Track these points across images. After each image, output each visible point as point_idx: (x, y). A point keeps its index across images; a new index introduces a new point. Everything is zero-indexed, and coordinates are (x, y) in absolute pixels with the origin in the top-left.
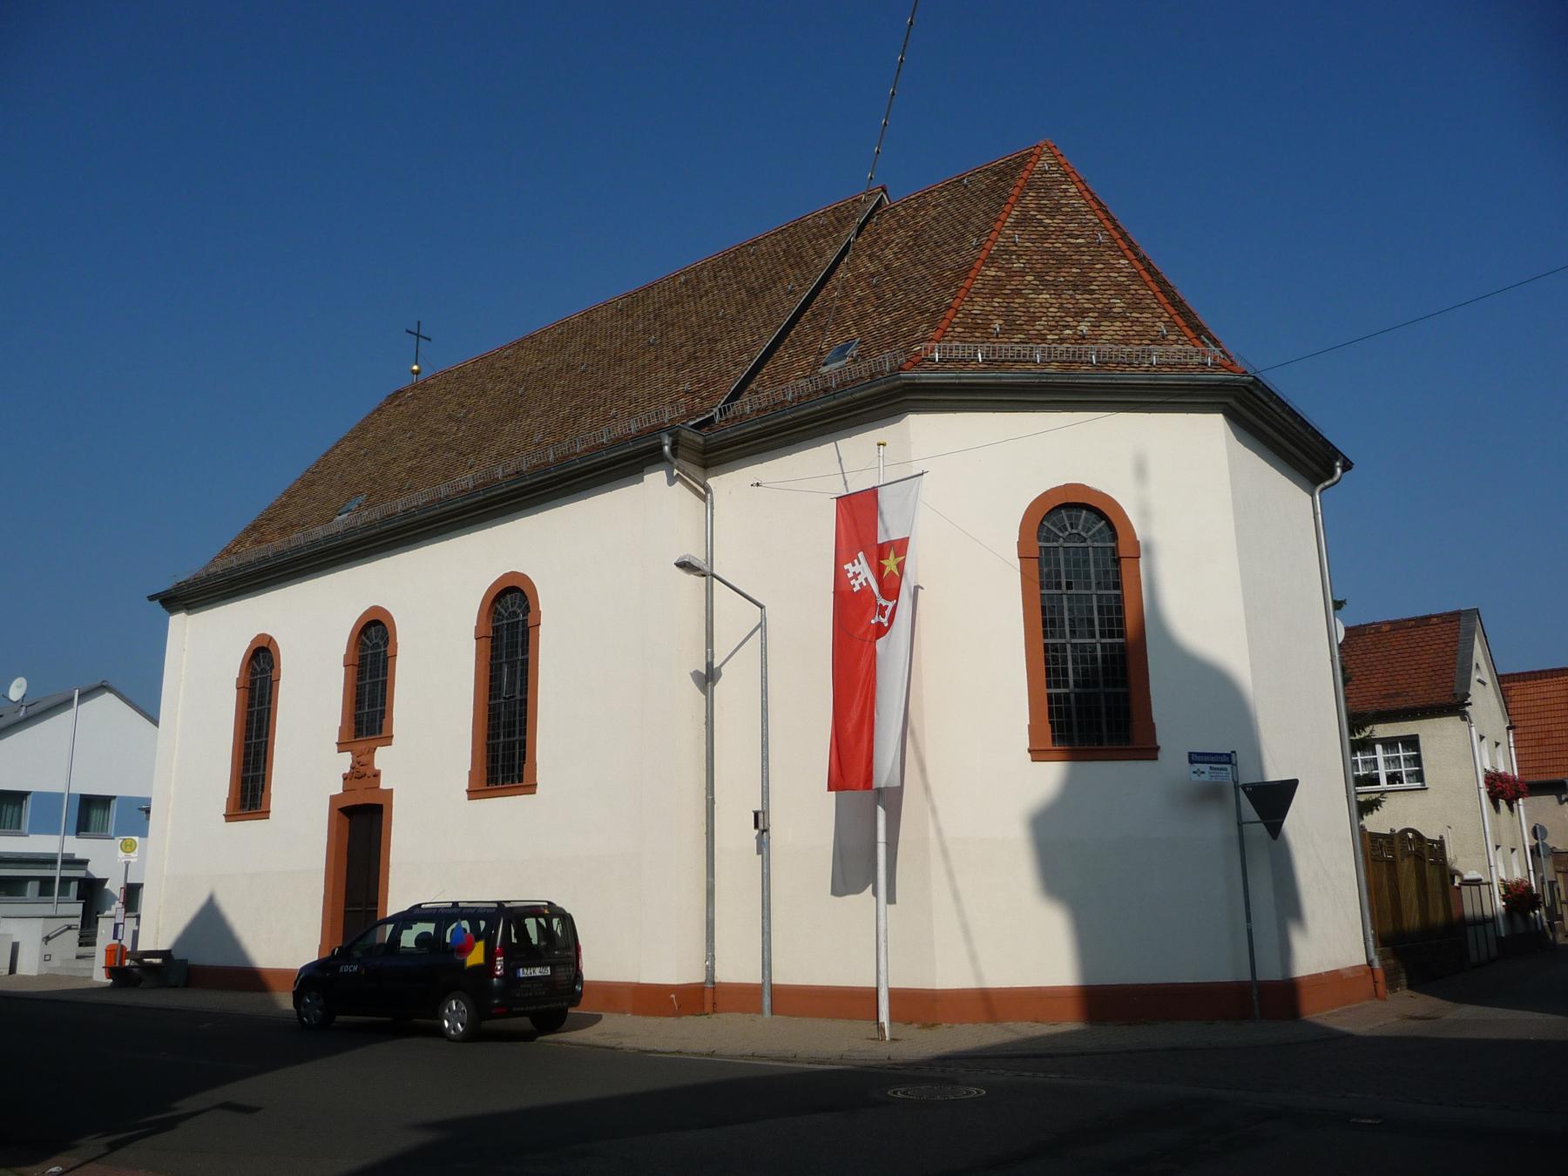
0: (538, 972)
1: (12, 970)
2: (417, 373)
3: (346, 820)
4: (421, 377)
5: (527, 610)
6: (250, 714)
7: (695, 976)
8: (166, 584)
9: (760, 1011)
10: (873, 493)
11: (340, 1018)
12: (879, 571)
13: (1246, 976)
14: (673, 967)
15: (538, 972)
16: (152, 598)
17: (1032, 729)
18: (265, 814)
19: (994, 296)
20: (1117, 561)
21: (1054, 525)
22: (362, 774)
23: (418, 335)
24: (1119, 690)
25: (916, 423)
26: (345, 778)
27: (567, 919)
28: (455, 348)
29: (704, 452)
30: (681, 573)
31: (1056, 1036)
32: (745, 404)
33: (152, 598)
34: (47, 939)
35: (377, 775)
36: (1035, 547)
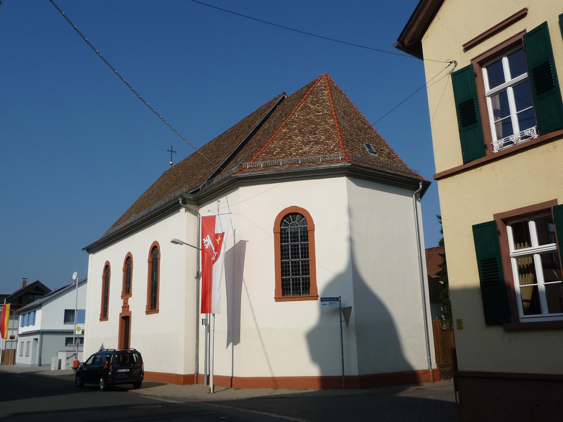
0: (124, 370)
1: (60, 368)
2: (172, 164)
3: (124, 321)
4: (173, 166)
5: (305, 222)
6: (129, 284)
7: (192, 372)
8: (87, 244)
9: (204, 383)
10: (214, 217)
11: (86, 384)
12: (215, 243)
13: (339, 373)
14: (181, 368)
15: (124, 370)
16: (83, 249)
17: (276, 291)
18: (157, 311)
19: (281, 140)
20: (307, 232)
21: (287, 221)
22: (126, 307)
23: (172, 151)
24: (298, 277)
25: (241, 189)
26: (122, 307)
27: (139, 354)
28: (184, 153)
29: (197, 201)
30: (174, 245)
31: (307, 393)
32: (215, 180)
33: (83, 249)
34: (68, 358)
35: (128, 307)
36: (158, 256)
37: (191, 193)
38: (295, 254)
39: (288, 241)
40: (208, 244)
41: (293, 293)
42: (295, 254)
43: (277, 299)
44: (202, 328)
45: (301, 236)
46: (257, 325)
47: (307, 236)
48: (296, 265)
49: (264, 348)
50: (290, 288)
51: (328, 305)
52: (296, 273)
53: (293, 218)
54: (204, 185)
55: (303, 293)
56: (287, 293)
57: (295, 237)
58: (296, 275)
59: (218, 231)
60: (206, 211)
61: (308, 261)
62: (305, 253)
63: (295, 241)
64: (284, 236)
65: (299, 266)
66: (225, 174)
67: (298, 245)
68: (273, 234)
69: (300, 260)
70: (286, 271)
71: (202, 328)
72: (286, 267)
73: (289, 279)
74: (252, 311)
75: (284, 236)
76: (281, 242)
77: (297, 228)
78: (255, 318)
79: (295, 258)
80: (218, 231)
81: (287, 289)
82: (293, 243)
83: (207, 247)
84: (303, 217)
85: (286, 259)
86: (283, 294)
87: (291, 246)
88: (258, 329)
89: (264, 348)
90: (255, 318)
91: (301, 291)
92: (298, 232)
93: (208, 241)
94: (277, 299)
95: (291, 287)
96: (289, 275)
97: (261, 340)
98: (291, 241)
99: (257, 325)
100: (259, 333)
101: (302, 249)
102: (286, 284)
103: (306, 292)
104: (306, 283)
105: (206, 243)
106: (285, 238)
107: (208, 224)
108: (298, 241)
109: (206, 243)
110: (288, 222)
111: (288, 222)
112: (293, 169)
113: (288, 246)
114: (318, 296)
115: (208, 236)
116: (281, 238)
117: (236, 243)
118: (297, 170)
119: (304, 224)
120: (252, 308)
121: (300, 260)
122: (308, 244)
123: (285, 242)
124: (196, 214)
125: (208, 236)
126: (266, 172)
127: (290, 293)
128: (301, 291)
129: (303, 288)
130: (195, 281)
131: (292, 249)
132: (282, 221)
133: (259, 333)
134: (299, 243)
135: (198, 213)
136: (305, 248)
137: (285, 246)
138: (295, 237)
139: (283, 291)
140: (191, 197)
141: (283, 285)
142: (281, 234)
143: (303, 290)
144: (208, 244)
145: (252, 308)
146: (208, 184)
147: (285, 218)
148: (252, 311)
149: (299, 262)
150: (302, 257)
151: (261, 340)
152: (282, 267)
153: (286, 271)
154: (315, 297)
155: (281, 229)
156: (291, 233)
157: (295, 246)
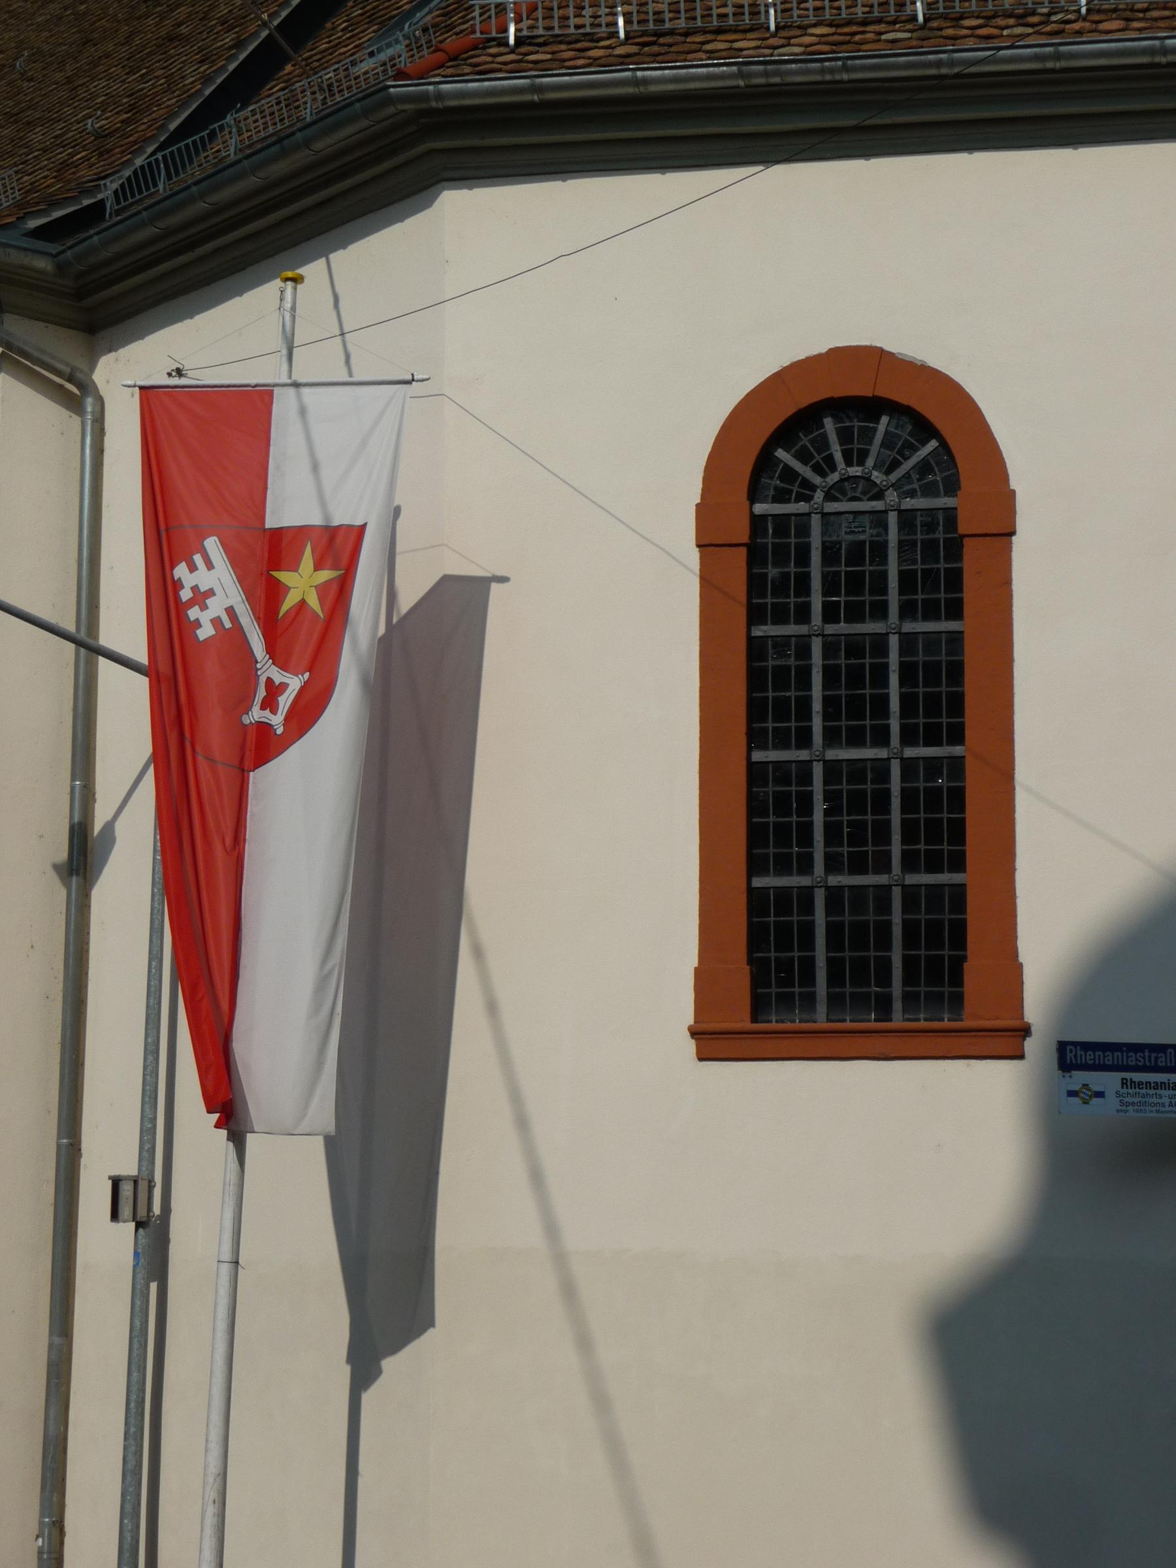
5: (943, 472)
12: (266, 596)
17: (704, 979)
20: (955, 548)
25: (458, 207)
37: (37, 233)
38: (856, 709)
39: (803, 614)
40: (216, 608)
41: (835, 1001)
42: (856, 709)
43: (713, 1041)
44: (106, 1246)
45: (907, 581)
46: (552, 1231)
47: (955, 580)
48: (858, 792)
49: (601, 1402)
50: (808, 966)
51: (1110, 1103)
52: (858, 844)
53: (845, 436)
54: (146, 176)
55: (910, 1000)
56: (786, 1001)
57: (855, 583)
58: (858, 865)
59: (290, 504)
60: (213, 342)
61: (957, 766)
62: (933, 703)
63: (855, 614)
64: (772, 572)
65: (882, 800)
66: (300, 96)
67: (880, 644)
68: (693, 557)
69: (893, 753)
70: (783, 832)
71: (106, 1246)
72: (782, 802)
73: (806, 895)
74: (522, 1123)
75: (772, 572)
76: (755, 615)
77: (879, 519)
78: (537, 1177)
79: (856, 739)
80: (290, 504)
81: (785, 966)
82: (843, 628)
83: (205, 632)
84: (925, 429)
85: (783, 744)
86: (759, 1008)
87: (830, 649)
88: (560, 1259)
89: (601, 1402)
90: (537, 1177)
91: (897, 988)
92: (880, 550)
93: (215, 585)
94: (713, 1041)
95: (897, 918)
96: (806, 866)
97: (584, 1343)
98: (830, 613)
99: (552, 1231)
100: (569, 1291)
101: (908, 673)
102: (784, 931)
103: (935, 1000)
104: (934, 928)
105: (201, 597)
106: (781, 587)
107: (206, 453)
108: (880, 611)
109: (201, 597)
110: (805, 471)
111: (805, 471)
112: (864, 66)
113: (804, 651)
114: (1025, 1031)
115: (212, 544)
116: (755, 584)
117: (406, 602)
118: (902, 65)
119: (930, 490)
120: (515, 1096)
121: (893, 753)
122: (956, 639)
123: (780, 616)
124: (75, 394)
125: (212, 544)
126: (658, 75)
127: (809, 1000)
128: (897, 988)
129: (910, 965)
130: (58, 894)
131: (830, 676)
132: (764, 462)
133: (569, 1291)
134: (892, 627)
135: (87, 387)
136: (932, 671)
137: (781, 644)
138: (855, 583)
139: (759, 980)
140: (43, 264)
141: (756, 937)
142: (755, 554)
143: (910, 977)
144: (216, 608)
145: (515, 1096)
146: (174, 166)
147: (784, 434)
148: (522, 1123)
149: (881, 770)
150: (909, 737)
151: (584, 1343)
152: (754, 806)
153: (783, 832)
154: (1007, 1040)
155: (757, 523)
156: (830, 553)
157: (855, 647)
